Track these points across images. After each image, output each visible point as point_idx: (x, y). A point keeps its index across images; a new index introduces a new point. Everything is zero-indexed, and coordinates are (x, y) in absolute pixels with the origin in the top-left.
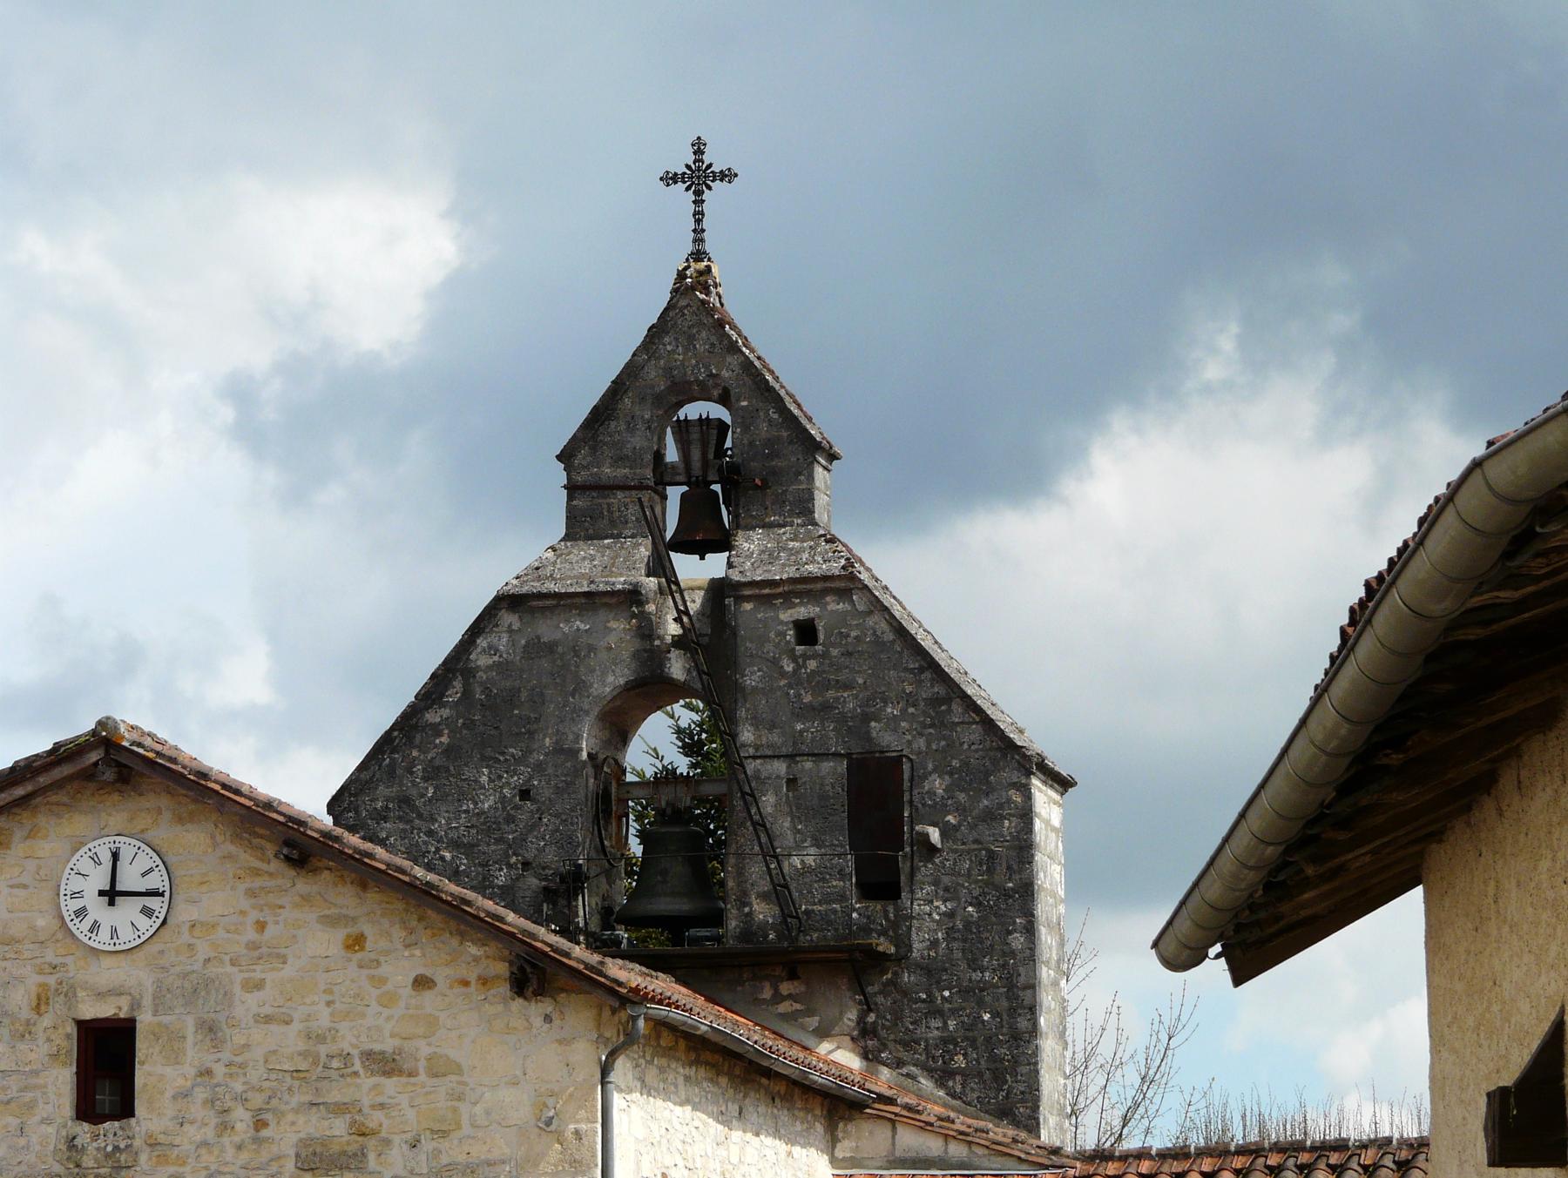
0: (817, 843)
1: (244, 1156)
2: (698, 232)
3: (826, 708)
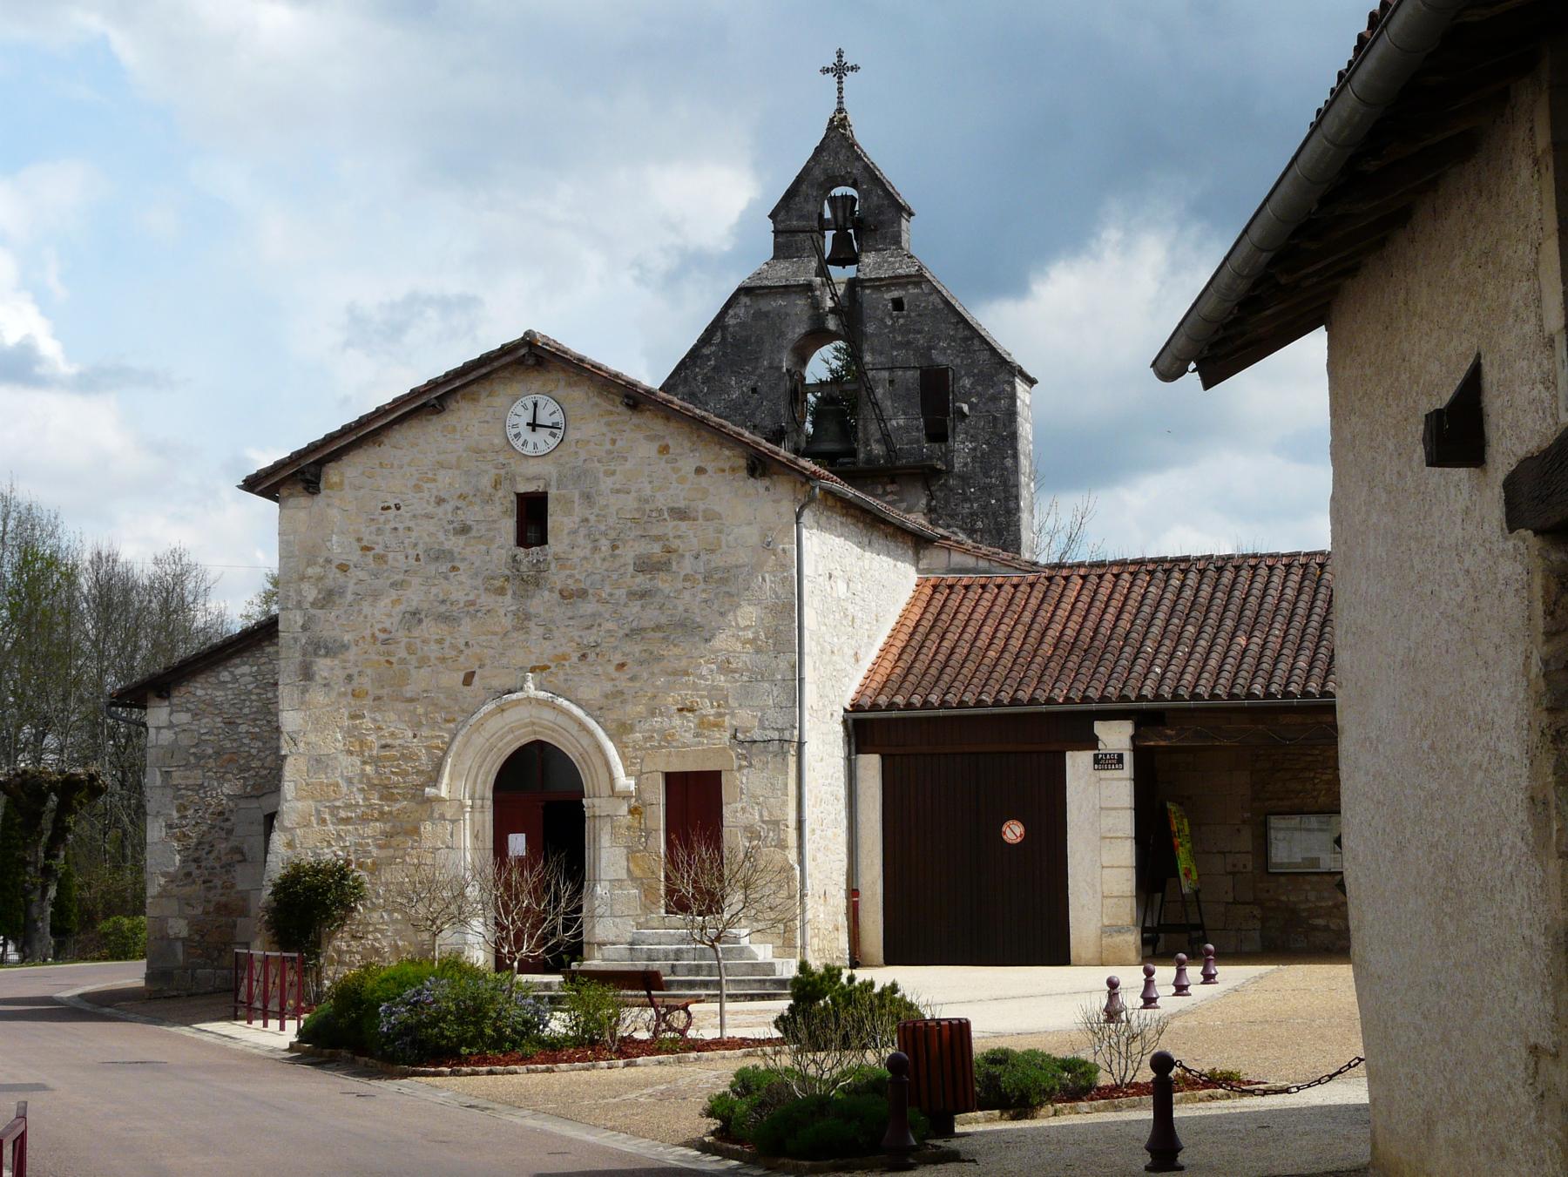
0: (905, 413)
1: (606, 564)
2: (840, 98)
3: (909, 343)
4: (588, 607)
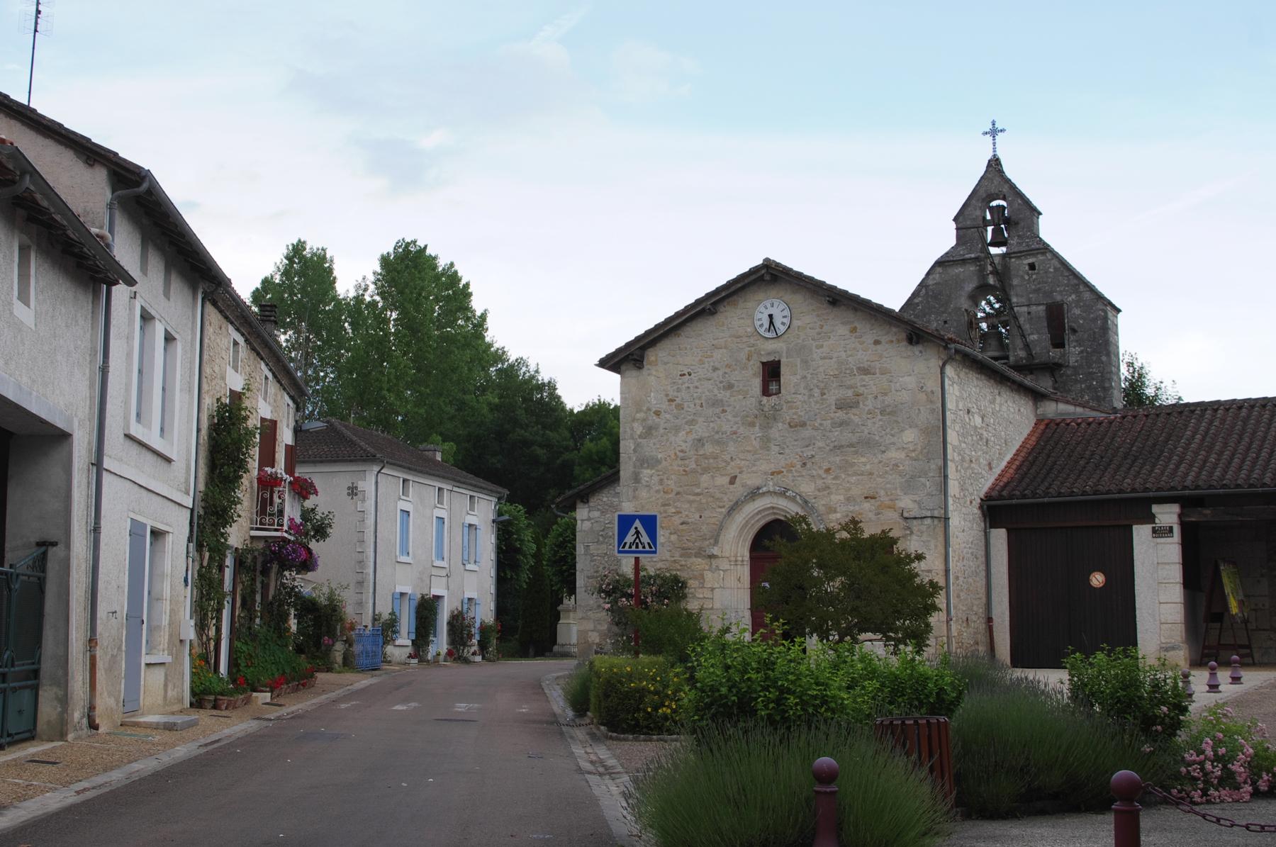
4: (807, 433)
